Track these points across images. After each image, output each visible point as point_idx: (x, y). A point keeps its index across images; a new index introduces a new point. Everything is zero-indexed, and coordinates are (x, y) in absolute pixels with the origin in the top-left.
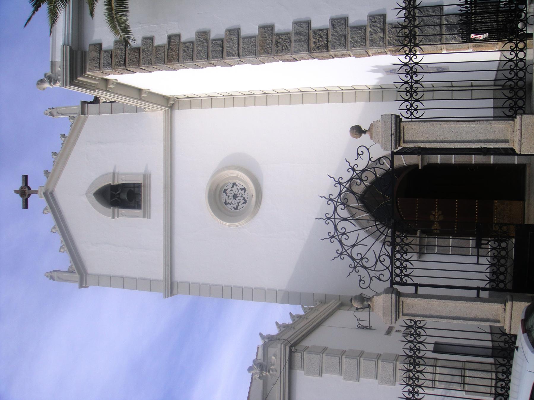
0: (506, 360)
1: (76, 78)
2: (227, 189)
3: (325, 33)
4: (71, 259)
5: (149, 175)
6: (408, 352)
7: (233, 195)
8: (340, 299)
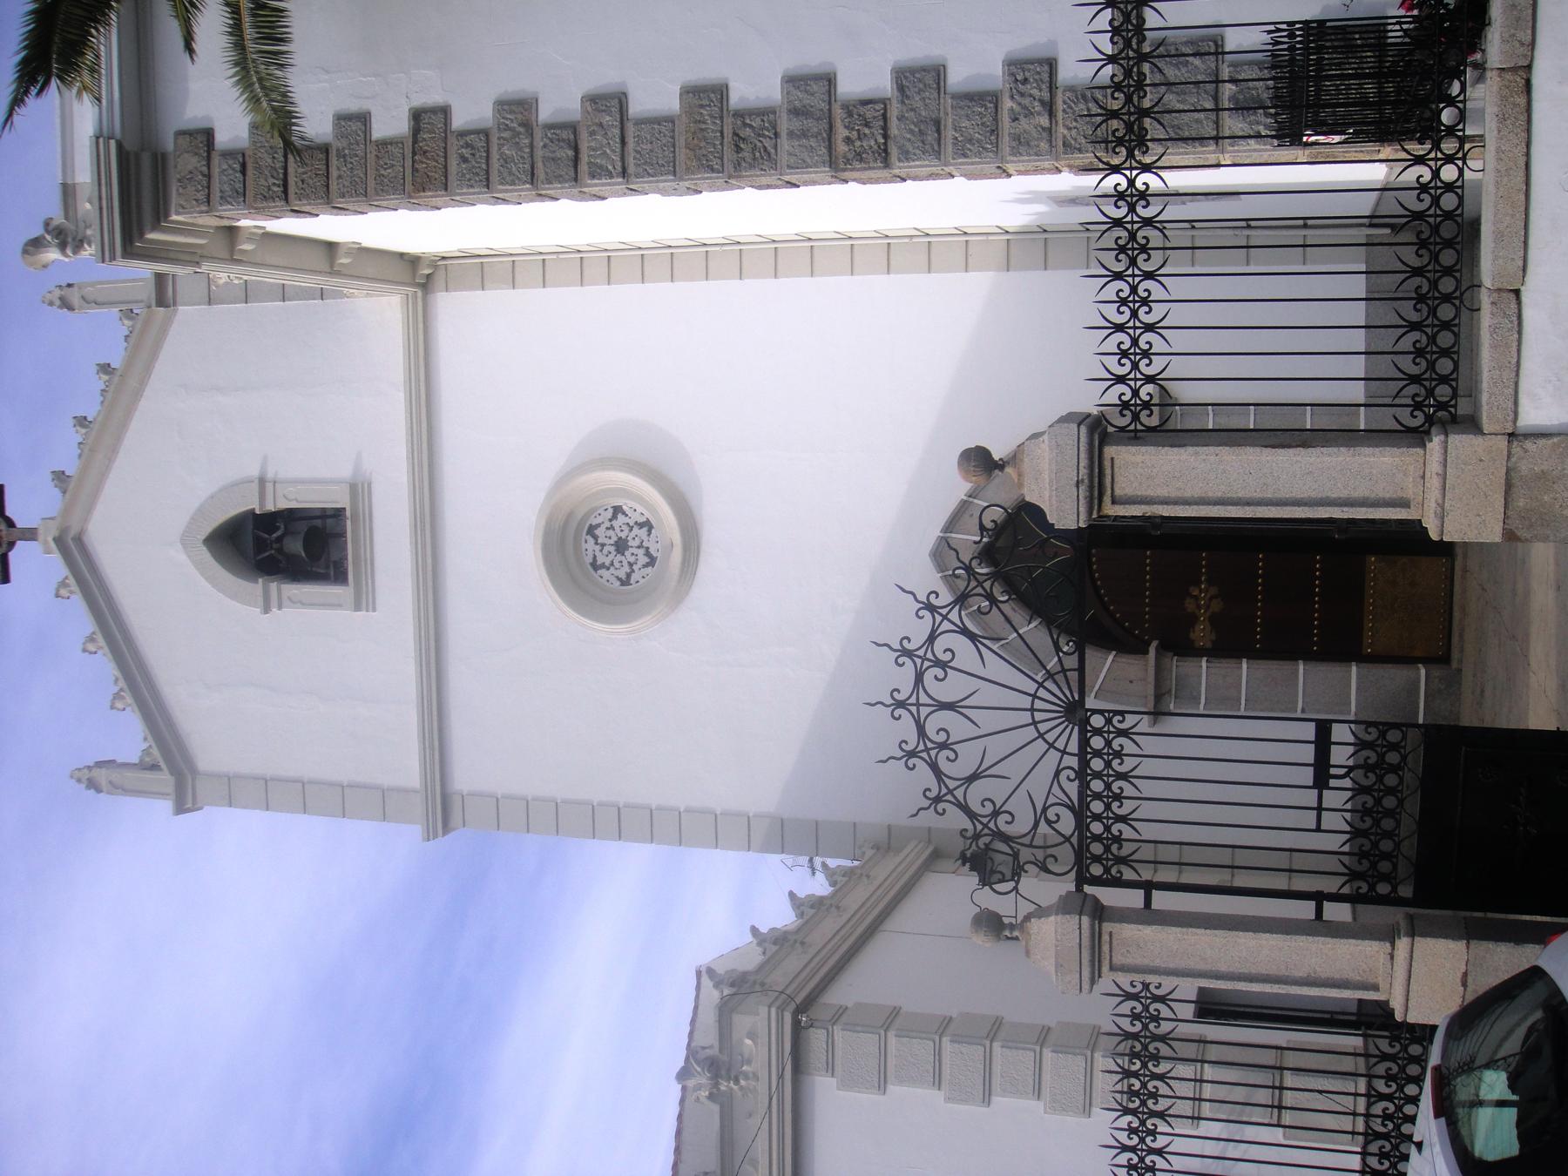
0: (1398, 1045)
1: (142, 234)
2: (598, 526)
3: (878, 111)
4: (147, 732)
5: (366, 486)
6: (1125, 1024)
7: (616, 542)
8: (929, 841)
